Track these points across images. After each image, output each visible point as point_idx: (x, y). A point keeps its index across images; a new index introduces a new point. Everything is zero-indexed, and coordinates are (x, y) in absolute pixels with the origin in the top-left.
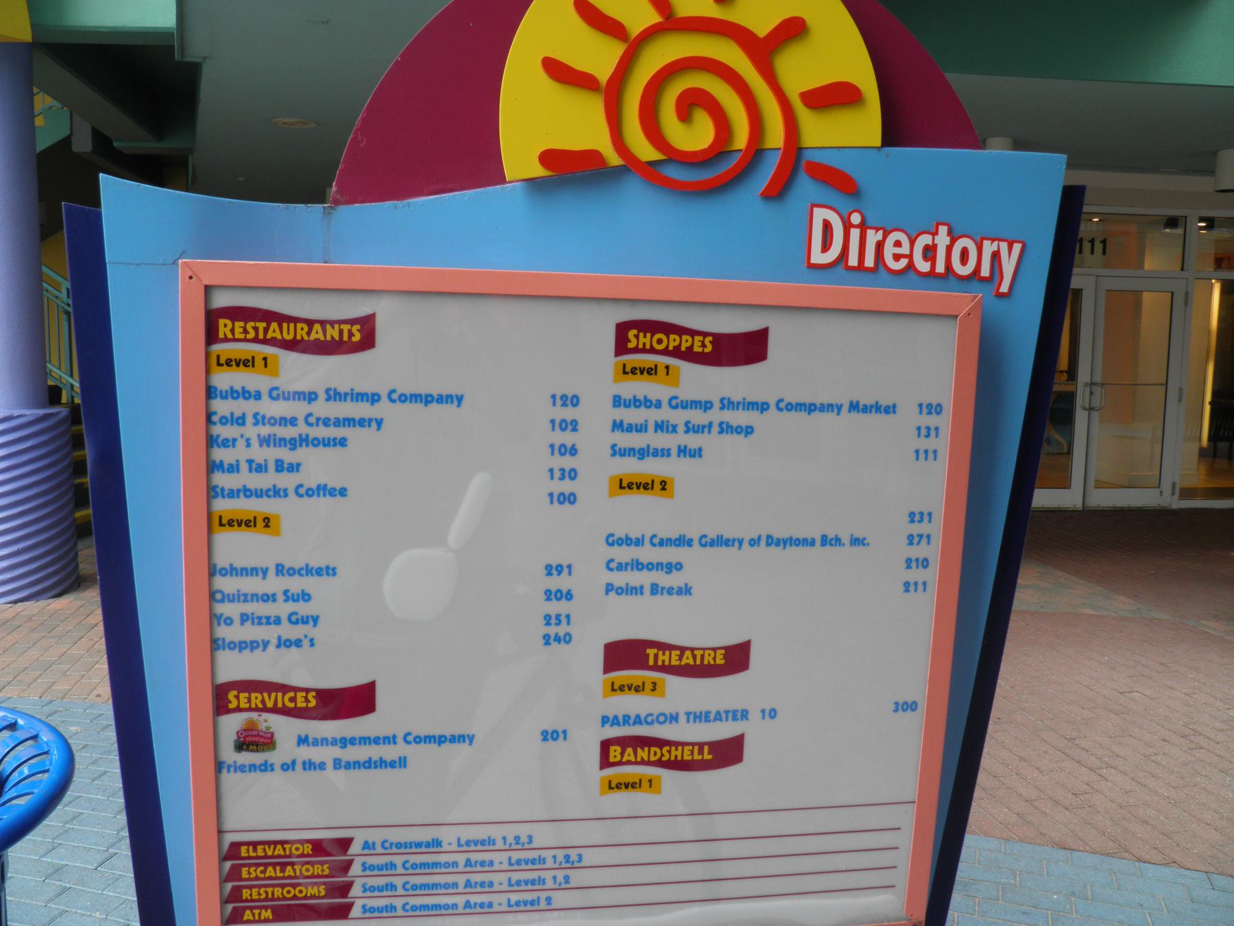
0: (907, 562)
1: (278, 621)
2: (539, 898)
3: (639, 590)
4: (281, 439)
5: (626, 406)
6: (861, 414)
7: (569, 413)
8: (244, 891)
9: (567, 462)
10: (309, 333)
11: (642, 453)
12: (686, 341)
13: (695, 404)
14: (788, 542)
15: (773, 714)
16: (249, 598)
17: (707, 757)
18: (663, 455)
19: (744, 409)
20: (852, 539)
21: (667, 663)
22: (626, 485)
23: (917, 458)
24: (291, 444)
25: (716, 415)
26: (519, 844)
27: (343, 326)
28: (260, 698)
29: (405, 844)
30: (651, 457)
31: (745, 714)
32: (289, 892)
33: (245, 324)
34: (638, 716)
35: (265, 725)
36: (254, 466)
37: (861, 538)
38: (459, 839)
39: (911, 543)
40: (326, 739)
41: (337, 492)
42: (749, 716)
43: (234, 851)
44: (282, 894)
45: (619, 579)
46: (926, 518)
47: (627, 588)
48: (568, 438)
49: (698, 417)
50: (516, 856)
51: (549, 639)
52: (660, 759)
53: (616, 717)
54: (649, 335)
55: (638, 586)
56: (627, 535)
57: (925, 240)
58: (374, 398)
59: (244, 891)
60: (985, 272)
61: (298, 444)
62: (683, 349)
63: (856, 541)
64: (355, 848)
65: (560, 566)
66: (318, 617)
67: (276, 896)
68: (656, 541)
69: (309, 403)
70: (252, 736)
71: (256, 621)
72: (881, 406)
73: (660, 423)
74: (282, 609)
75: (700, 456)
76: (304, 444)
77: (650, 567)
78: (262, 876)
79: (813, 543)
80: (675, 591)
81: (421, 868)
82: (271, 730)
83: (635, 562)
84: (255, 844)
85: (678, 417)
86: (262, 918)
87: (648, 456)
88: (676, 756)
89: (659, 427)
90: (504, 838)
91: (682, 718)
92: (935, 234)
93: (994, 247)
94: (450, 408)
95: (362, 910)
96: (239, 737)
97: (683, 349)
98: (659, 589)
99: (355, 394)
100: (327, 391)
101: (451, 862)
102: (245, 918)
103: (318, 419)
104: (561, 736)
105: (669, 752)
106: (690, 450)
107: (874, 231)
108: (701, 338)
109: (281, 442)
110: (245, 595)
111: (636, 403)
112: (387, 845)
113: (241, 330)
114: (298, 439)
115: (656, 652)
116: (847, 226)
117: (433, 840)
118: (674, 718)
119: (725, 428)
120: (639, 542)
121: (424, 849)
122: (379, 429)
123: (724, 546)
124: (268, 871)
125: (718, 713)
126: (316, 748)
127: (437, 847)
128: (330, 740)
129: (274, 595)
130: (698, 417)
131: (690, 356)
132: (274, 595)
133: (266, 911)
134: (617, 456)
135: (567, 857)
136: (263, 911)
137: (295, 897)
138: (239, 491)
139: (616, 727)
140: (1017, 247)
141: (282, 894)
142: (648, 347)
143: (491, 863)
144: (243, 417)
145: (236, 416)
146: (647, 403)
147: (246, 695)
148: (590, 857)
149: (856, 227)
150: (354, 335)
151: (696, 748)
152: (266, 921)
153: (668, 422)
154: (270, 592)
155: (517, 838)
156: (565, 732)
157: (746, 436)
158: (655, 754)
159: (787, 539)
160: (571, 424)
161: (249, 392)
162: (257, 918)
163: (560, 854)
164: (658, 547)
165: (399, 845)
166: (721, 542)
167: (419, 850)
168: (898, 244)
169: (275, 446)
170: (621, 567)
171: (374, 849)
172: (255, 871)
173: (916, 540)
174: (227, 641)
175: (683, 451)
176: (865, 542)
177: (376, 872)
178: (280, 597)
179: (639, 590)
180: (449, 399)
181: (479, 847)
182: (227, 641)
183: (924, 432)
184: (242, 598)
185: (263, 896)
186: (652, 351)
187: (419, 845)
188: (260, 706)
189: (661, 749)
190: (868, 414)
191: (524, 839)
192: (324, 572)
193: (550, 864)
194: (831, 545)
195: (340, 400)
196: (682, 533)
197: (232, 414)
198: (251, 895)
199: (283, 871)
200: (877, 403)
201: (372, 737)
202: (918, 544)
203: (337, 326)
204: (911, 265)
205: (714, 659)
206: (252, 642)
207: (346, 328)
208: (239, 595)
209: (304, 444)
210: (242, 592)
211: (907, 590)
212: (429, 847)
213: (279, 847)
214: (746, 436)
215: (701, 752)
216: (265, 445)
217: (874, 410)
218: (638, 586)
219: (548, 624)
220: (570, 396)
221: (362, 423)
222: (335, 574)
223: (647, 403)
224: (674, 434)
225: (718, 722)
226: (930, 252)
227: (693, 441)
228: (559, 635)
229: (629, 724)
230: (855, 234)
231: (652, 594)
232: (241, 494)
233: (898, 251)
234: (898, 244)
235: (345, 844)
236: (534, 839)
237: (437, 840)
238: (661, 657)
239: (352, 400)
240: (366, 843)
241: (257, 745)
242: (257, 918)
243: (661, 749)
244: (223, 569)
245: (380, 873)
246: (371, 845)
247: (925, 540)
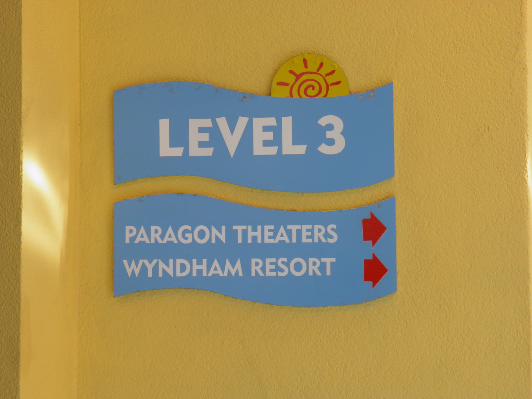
10: (162, 237)
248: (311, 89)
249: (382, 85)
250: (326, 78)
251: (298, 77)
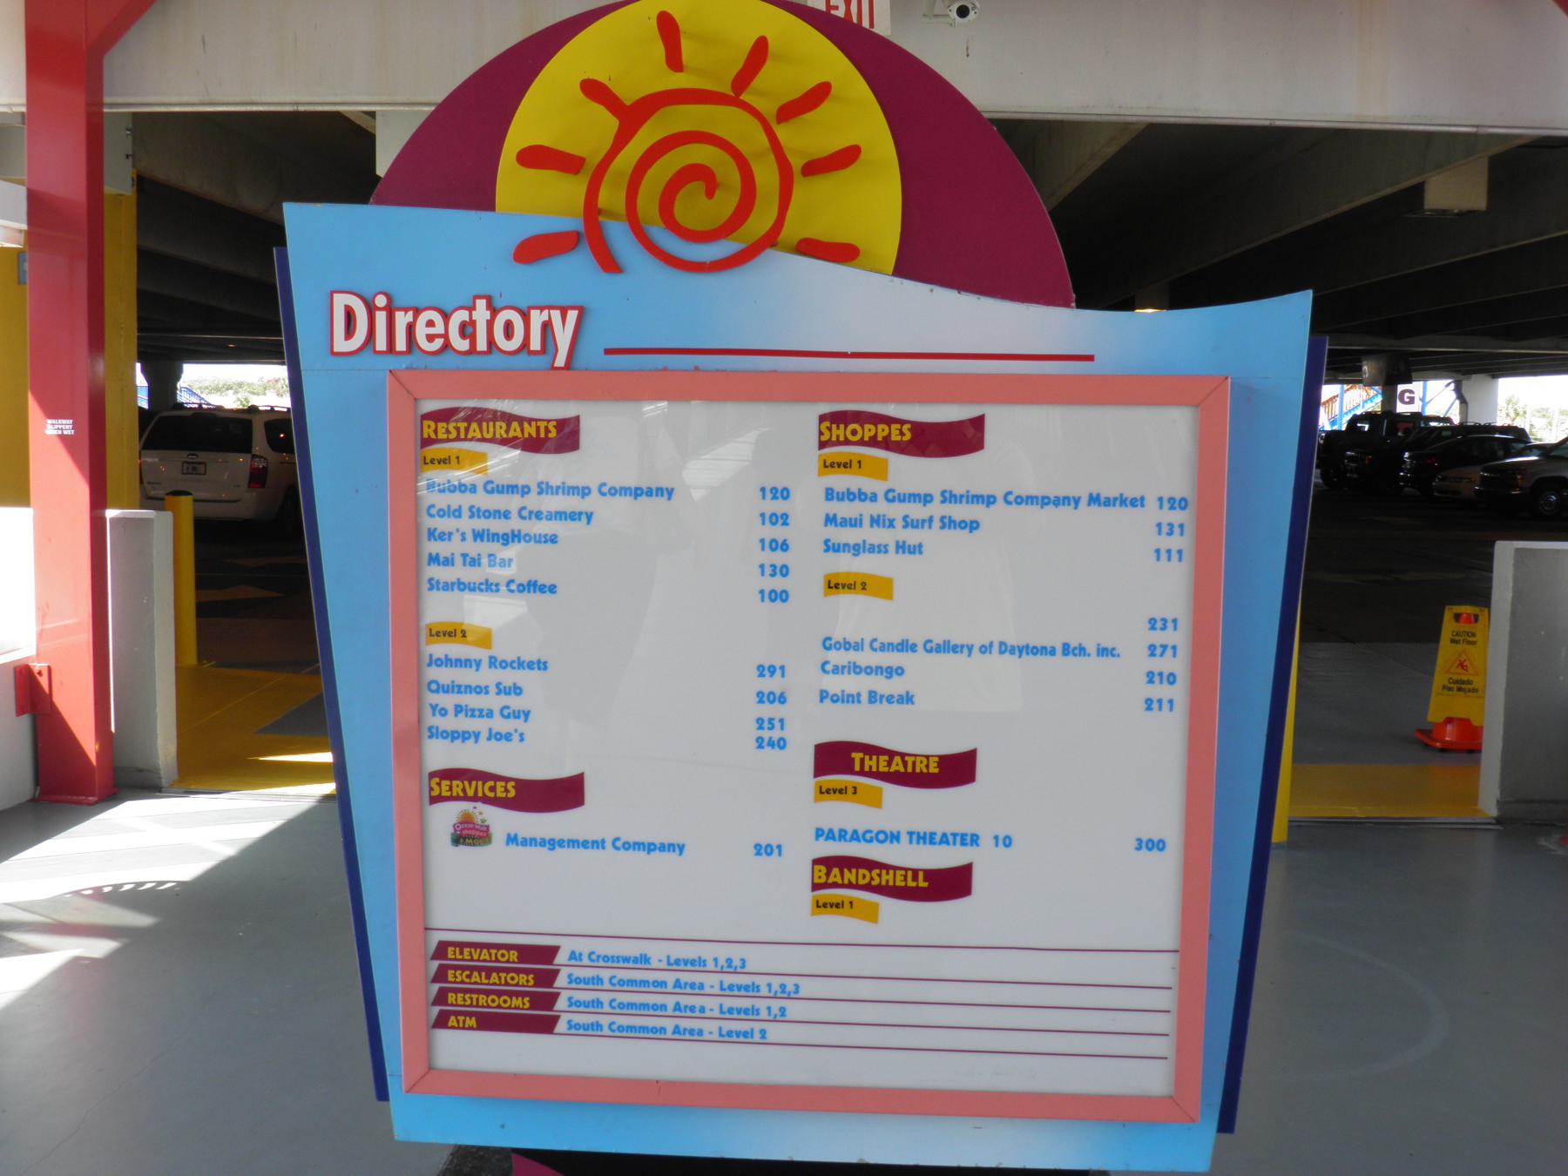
0: (1148, 675)
1: (490, 714)
2: (752, 1029)
3: (856, 699)
4: (494, 535)
5: (839, 499)
6: (1103, 507)
7: (779, 506)
8: (450, 995)
9: (779, 558)
10: (507, 431)
11: (857, 549)
12: (882, 431)
13: (914, 497)
14: (1024, 651)
15: (1007, 841)
16: (463, 689)
17: (923, 884)
18: (879, 552)
19: (967, 502)
20: (1098, 649)
22: (834, 585)
23: (1158, 559)
24: (503, 539)
25: (937, 509)
28: (461, 787)
29: (613, 957)
30: (867, 554)
31: (975, 840)
32: (493, 1001)
33: (901, 427)
34: (855, 832)
35: (480, 817)
36: (468, 560)
37: (1110, 647)
39: (1152, 654)
40: (535, 839)
41: (547, 589)
42: (979, 842)
43: (442, 950)
44: (487, 1002)
45: (835, 684)
46: (1170, 625)
47: (843, 695)
48: (779, 533)
49: (917, 511)
50: (729, 979)
51: (762, 743)
52: (870, 883)
53: (831, 831)
54: (842, 426)
55: (855, 693)
56: (844, 639)
57: (462, 316)
58: (584, 492)
59: (450, 995)
60: (535, 344)
61: (510, 540)
62: (880, 438)
63: (1104, 652)
64: (561, 958)
65: (773, 666)
66: (529, 712)
67: (480, 1004)
68: (876, 645)
69: (522, 496)
70: (468, 829)
71: (469, 713)
72: (1126, 499)
73: (876, 518)
74: (493, 701)
75: (921, 553)
76: (516, 539)
77: (869, 670)
78: (468, 980)
79: (1053, 652)
80: (895, 699)
82: (486, 824)
83: (852, 665)
84: (461, 945)
85: (896, 511)
86: (467, 1026)
87: (864, 551)
88: (887, 881)
89: (875, 521)
90: (716, 960)
91: (905, 838)
92: (471, 309)
94: (660, 502)
95: (567, 1026)
96: (456, 831)
97: (880, 438)
98: (878, 697)
99: (566, 489)
100: (943, 493)
102: (450, 1024)
103: (531, 512)
104: (776, 851)
105: (880, 875)
106: (909, 546)
107: (539, 311)
108: (898, 426)
109: (494, 537)
110: (459, 686)
111: (850, 496)
112: (594, 957)
114: (510, 535)
116: (371, 309)
118: (895, 837)
119: (948, 523)
120: (858, 646)
121: (631, 965)
122: (588, 523)
123: (909, 652)
124: (474, 976)
125: (944, 835)
126: (525, 848)
127: (645, 963)
128: (539, 840)
129: (486, 687)
130: (917, 511)
132: (486, 687)
133: (471, 1019)
134: (831, 552)
135: (783, 986)
136: (468, 1018)
137: (499, 1007)
138: (453, 584)
139: (830, 842)
141: (487, 1002)
142: (842, 439)
144: (459, 510)
145: (453, 508)
146: (861, 496)
147: (448, 782)
148: (808, 988)
149: (381, 309)
150: (550, 432)
151: (910, 873)
152: (471, 1028)
153: (884, 516)
154: (483, 684)
155: (729, 961)
156: (779, 847)
157: (971, 532)
158: (864, 876)
159: (1023, 647)
160: (782, 518)
161: (865, 494)
162: (461, 1025)
164: (878, 652)
165: (606, 958)
166: (947, 647)
167: (626, 965)
169: (488, 540)
170: (837, 670)
171: (581, 960)
172: (461, 975)
173: (1159, 651)
174: (441, 730)
175: (901, 547)
176: (1114, 652)
177: (582, 986)
178: (493, 690)
179: (856, 699)
180: (660, 492)
181: (689, 967)
182: (441, 730)
183: (1165, 529)
184: (456, 689)
185: (468, 1003)
186: (847, 442)
187: (626, 960)
188: (461, 794)
189: (870, 872)
190: (1111, 507)
191: (737, 963)
192: (536, 666)
194: (1075, 655)
195: (956, 502)
196: (905, 638)
197: (449, 507)
198: (456, 1000)
199: (488, 977)
200: (1121, 495)
201: (581, 840)
202: (1162, 655)
203: (533, 423)
204: (447, 345)
206: (464, 733)
208: (453, 686)
209: (516, 539)
210: (456, 683)
211: (1149, 708)
212: (637, 963)
213: (485, 951)
215: (915, 878)
216: (478, 540)
217: (1118, 502)
218: (855, 693)
219: (760, 728)
220: (780, 489)
221: (574, 516)
222: (545, 668)
223: (861, 496)
224: (891, 529)
225: (944, 845)
226: (467, 329)
227: (912, 536)
228: (773, 739)
229: (845, 840)
230: (381, 318)
231: (870, 702)
232: (455, 587)
233: (431, 331)
235: (554, 950)
236: (747, 964)
237: (646, 955)
238: (867, 763)
239: (967, 502)
240: (573, 953)
241: (473, 839)
242: (461, 1025)
243: (870, 872)
244: (439, 659)
245: (587, 987)
246: (577, 956)
247: (1169, 652)
248: (696, 188)
249: (1183, 504)
250: (782, 132)
251: (631, 116)
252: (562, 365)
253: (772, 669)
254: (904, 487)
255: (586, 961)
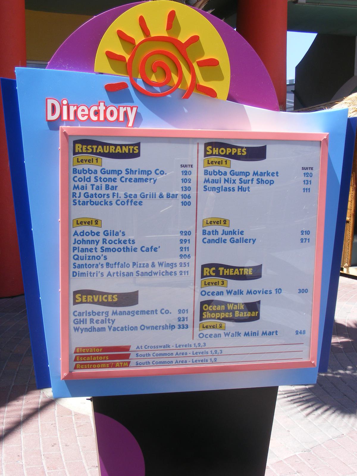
10: (115, 150)
12: (234, 151)
21: (228, 274)
26: (200, 346)
27: (130, 147)
33: (87, 146)
38: (176, 345)
54: (217, 149)
62: (233, 154)
78: (85, 360)
81: (159, 356)
93: (125, 109)
97: (233, 154)
99: (140, 171)
100: (126, 170)
101: (159, 354)
107: (73, 106)
111: (214, 173)
113: (85, 149)
115: (223, 269)
117: (166, 345)
131: (236, 157)
135: (216, 351)
140: (135, 109)
143: (186, 354)
148: (225, 351)
149: (65, 105)
163: (213, 350)
168: (83, 110)
191: (202, 344)
193: (210, 354)
205: (248, 272)
207: (131, 148)
214: (270, 185)
230: (65, 108)
233: (83, 113)
234: (83, 110)
238: (225, 272)
242: (121, 366)
252: (131, 126)
253: (185, 241)
254: (237, 170)
255: (144, 349)
